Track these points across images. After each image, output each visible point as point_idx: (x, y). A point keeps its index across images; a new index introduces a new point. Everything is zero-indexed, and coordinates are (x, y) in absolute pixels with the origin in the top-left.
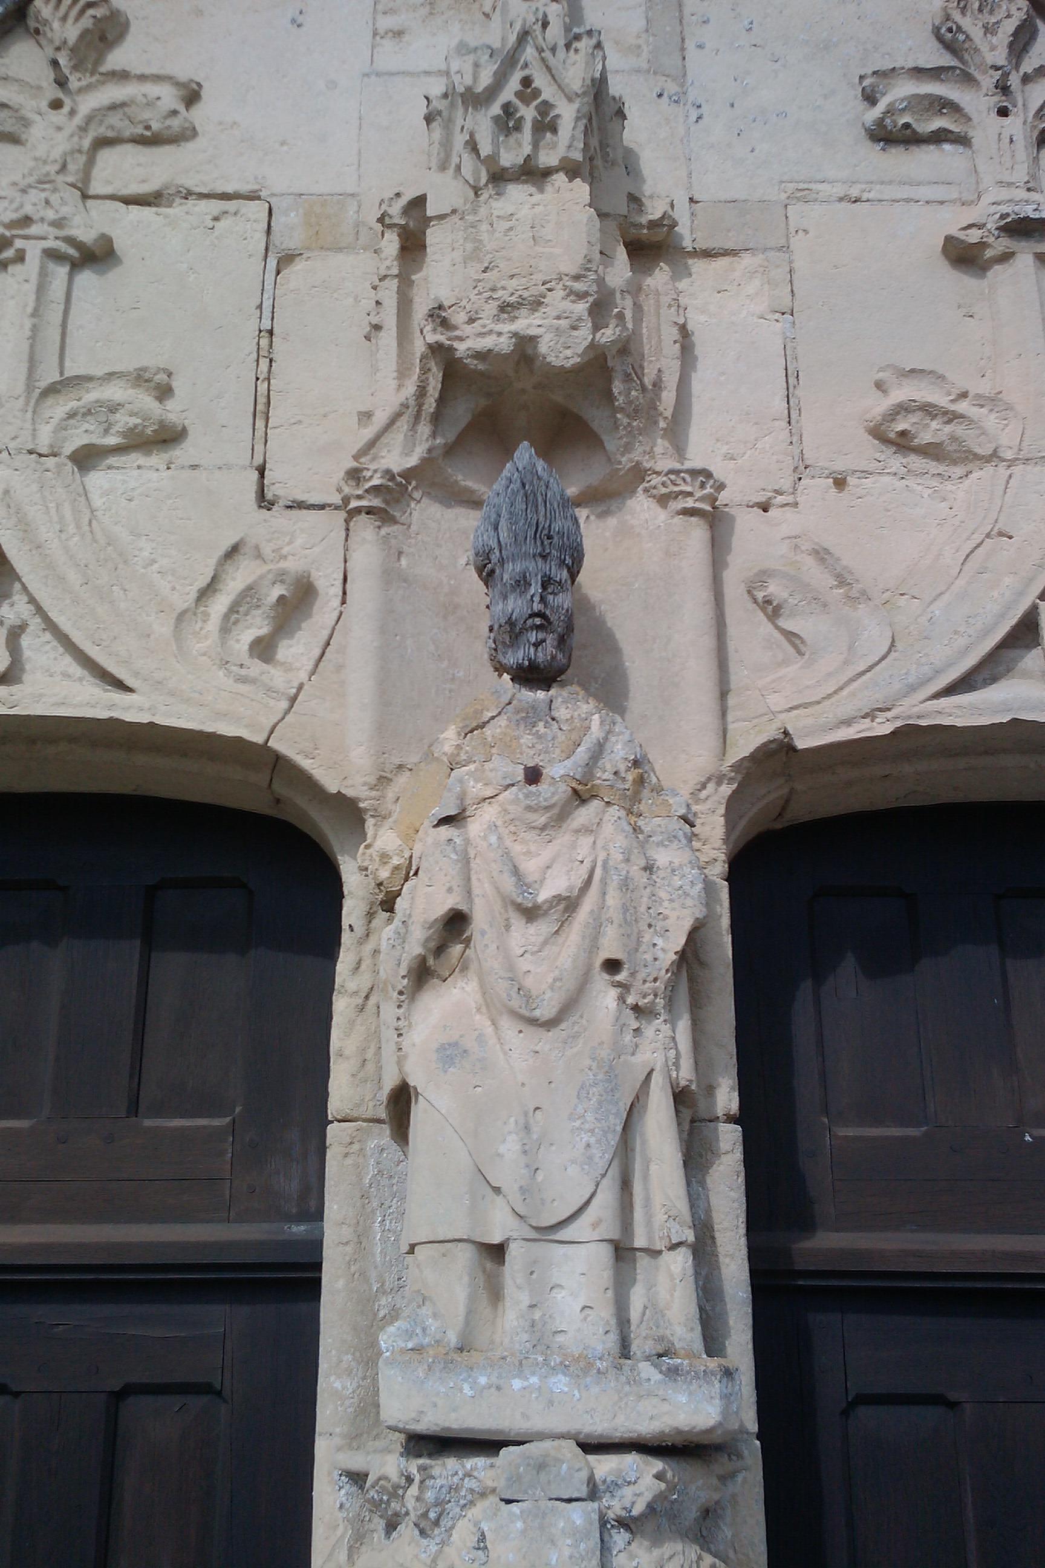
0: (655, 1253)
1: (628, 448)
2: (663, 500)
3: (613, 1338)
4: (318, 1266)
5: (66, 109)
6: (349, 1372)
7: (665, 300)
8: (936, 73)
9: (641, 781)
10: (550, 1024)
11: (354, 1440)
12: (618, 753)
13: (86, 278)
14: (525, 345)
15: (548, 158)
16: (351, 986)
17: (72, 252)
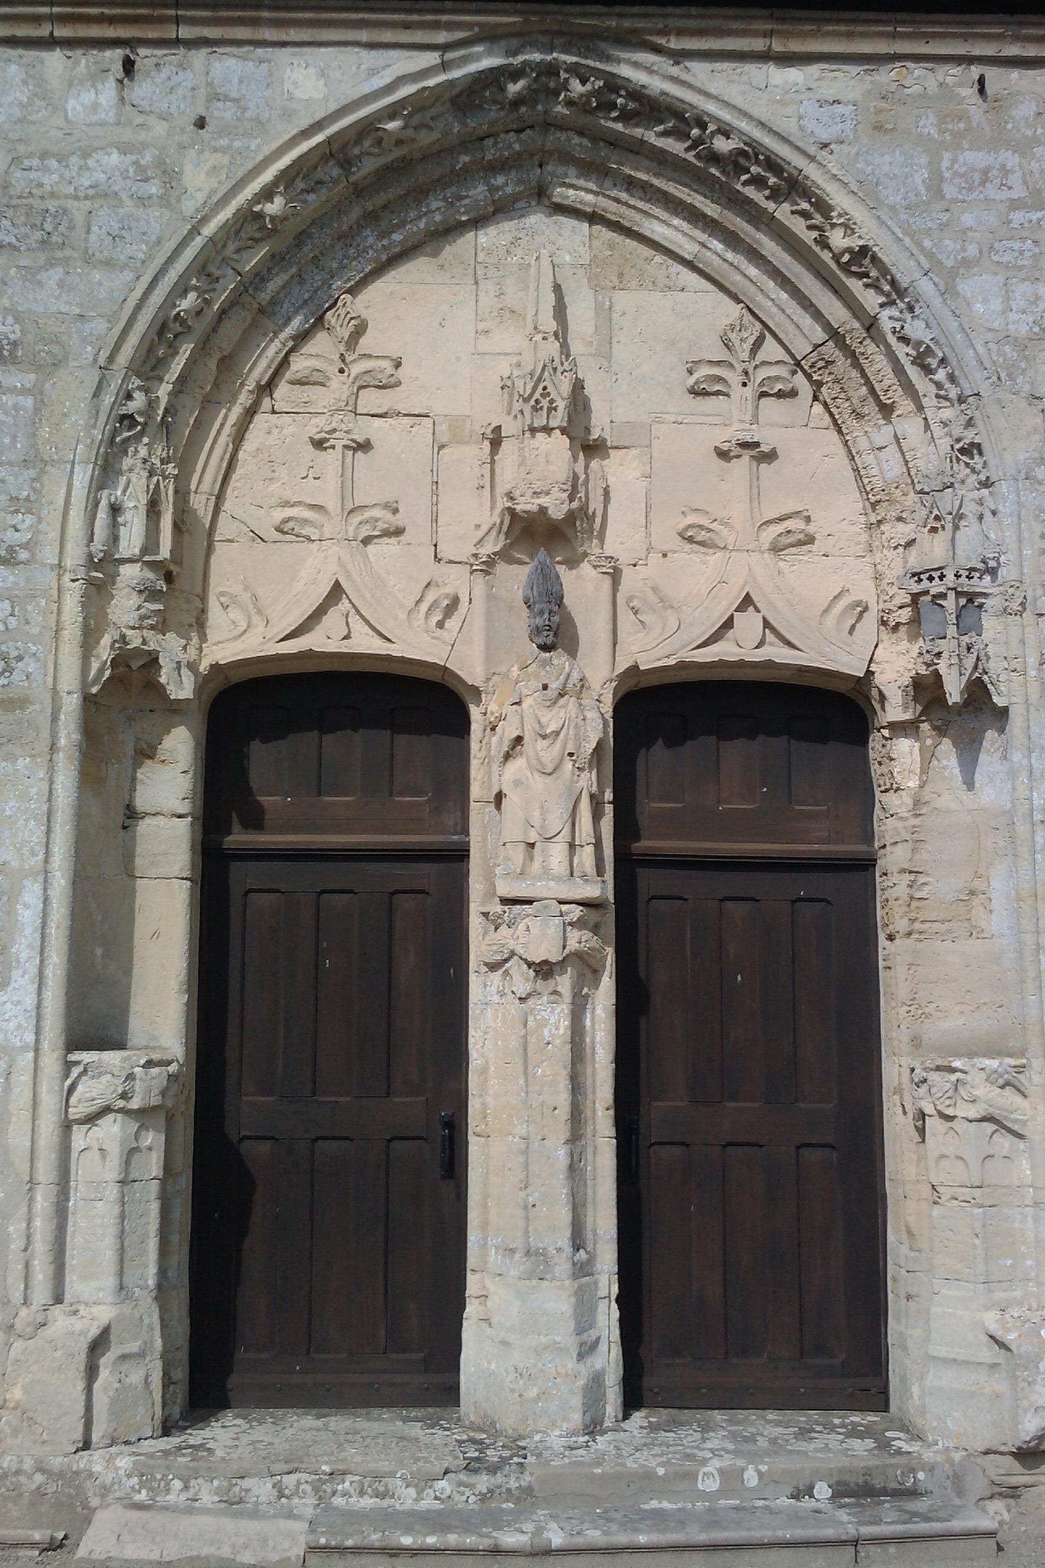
0: (582, 846)
1: (582, 545)
2: (595, 567)
3: (568, 871)
4: (468, 851)
5: (346, 374)
6: (481, 883)
7: (599, 476)
8: (719, 363)
9: (583, 686)
10: (550, 774)
11: (484, 903)
12: (575, 676)
13: (359, 454)
14: (543, 510)
15: (553, 423)
16: (479, 755)
17: (354, 445)
